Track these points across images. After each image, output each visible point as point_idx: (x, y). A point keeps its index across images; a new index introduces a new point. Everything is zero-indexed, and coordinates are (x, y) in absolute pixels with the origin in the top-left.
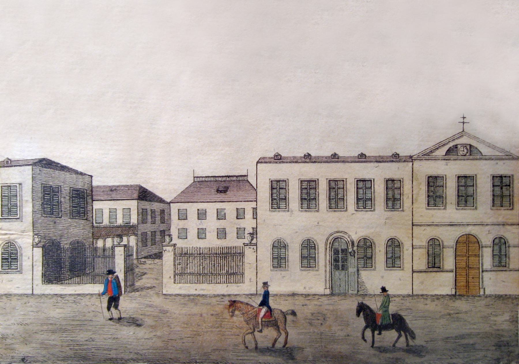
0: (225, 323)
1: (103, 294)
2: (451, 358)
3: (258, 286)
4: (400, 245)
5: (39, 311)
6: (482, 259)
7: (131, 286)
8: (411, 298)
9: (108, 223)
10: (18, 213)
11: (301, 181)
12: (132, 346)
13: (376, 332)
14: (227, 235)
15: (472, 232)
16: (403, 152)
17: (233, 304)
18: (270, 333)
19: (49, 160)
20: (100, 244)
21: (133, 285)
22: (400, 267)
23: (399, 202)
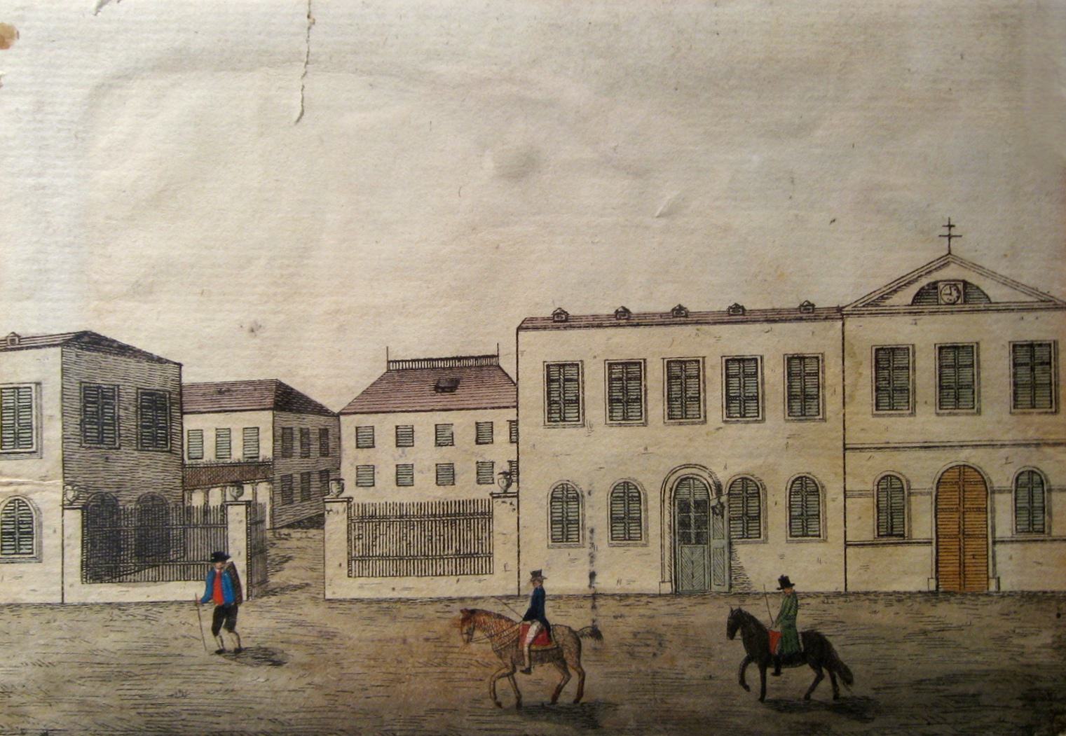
0: (454, 655)
1: (205, 601)
2: (929, 724)
3: (521, 580)
4: (818, 491)
5: (75, 638)
6: (993, 518)
8: (842, 599)
9: (213, 459)
10: (34, 441)
11: (610, 365)
12: (261, 707)
13: (770, 671)
14: (456, 477)
15: (972, 462)
16: (823, 301)
17: (471, 617)
18: (547, 674)
19: (95, 334)
20: (197, 500)
21: (264, 581)
22: (819, 536)
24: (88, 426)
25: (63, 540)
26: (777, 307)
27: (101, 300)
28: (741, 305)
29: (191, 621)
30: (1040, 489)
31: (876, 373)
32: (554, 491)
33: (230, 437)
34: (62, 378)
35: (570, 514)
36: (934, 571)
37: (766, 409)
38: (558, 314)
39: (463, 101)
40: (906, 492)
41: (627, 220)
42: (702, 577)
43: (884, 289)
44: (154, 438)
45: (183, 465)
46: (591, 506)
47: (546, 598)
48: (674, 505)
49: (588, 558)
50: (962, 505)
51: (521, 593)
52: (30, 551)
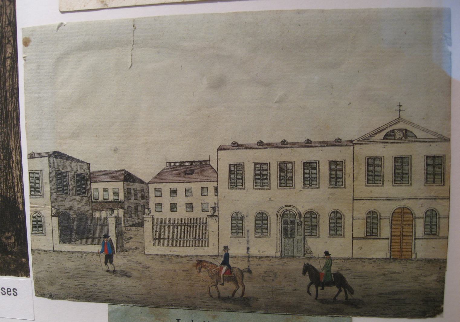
0: (194, 277)
1: (101, 252)
2: (384, 310)
3: (220, 249)
4: (341, 217)
5: (58, 263)
6: (415, 229)
7: (121, 247)
8: (350, 260)
9: (102, 200)
10: (41, 192)
11: (255, 164)
12: (124, 291)
13: (320, 288)
14: (194, 209)
15: (408, 205)
16: (345, 138)
17: (200, 263)
18: (230, 286)
19: (59, 152)
20: (97, 215)
21: (122, 246)
22: (342, 235)
23: (341, 181)
24: (58, 187)
25: (52, 228)
26: (326, 140)
27: (61, 139)
28: (310, 139)
29: (97, 259)
30: (435, 217)
31: (367, 168)
32: (232, 215)
33: (108, 191)
34: (49, 169)
35: (239, 224)
36: (389, 250)
37: (320, 183)
38: (234, 143)
39: (195, 57)
40: (379, 218)
41: (262, 104)
42: (293, 251)
43: (371, 133)
44: (81, 192)
45: (92, 202)
46: (248, 221)
47: (230, 257)
48: (281, 222)
49: (246, 242)
50: (402, 223)
51: (220, 255)
52: (42, 231)
